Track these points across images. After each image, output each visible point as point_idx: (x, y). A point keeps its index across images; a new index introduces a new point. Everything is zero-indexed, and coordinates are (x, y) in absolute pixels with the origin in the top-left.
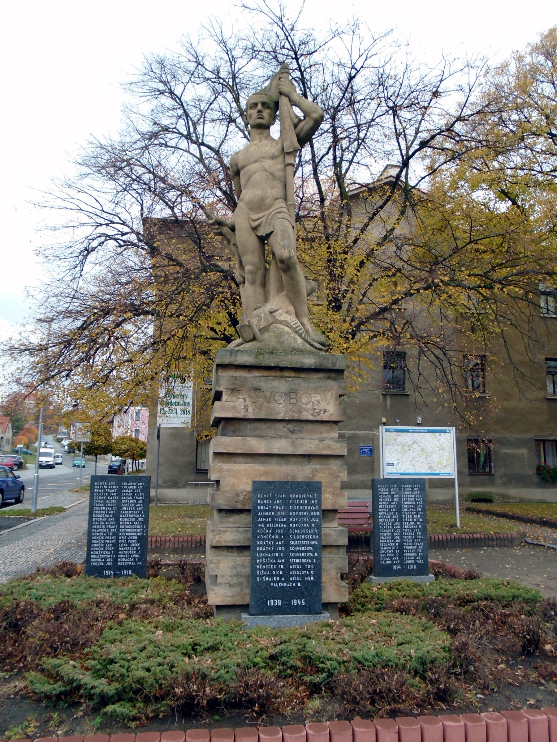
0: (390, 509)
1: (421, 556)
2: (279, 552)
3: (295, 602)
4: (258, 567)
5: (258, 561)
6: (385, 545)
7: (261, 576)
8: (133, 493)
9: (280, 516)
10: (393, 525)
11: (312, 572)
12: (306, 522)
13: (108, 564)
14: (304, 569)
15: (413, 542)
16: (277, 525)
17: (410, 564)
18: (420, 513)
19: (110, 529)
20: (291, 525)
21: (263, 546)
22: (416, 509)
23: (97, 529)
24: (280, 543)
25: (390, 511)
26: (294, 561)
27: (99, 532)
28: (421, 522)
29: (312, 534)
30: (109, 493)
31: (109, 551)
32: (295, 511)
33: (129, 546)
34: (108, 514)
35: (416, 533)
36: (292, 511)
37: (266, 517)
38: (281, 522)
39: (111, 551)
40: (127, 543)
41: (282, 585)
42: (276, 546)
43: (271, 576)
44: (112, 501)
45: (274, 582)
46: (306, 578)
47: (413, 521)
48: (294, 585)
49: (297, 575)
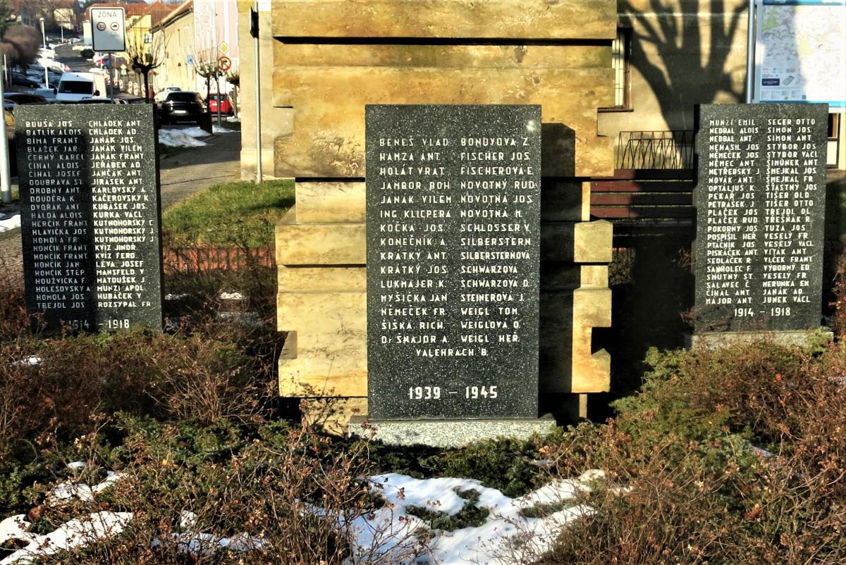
0: (735, 178)
1: (805, 289)
2: (434, 277)
3: (474, 392)
4: (384, 312)
5: (383, 298)
6: (719, 261)
7: (391, 334)
8: (117, 145)
9: (438, 192)
10: (740, 216)
11: (516, 325)
12: (501, 207)
13: (76, 305)
14: (495, 316)
15: (788, 255)
16: (429, 213)
17: (777, 305)
18: (810, 187)
19: (71, 230)
20: (463, 214)
21: (394, 263)
22: (800, 177)
23: (41, 229)
24: (437, 256)
25: (735, 183)
26: (471, 297)
27: (48, 236)
28: (811, 209)
29: (517, 236)
30: (61, 147)
31: (74, 277)
32: (474, 179)
33: (118, 266)
34: (63, 194)
35: (796, 233)
36: (465, 178)
37: (400, 193)
38: (440, 207)
39: (79, 278)
40: (113, 259)
41: (443, 352)
42: (426, 264)
43: (417, 332)
44: (69, 165)
45: (422, 347)
46: (501, 339)
47: (791, 206)
48: (471, 353)
49: (477, 332)
